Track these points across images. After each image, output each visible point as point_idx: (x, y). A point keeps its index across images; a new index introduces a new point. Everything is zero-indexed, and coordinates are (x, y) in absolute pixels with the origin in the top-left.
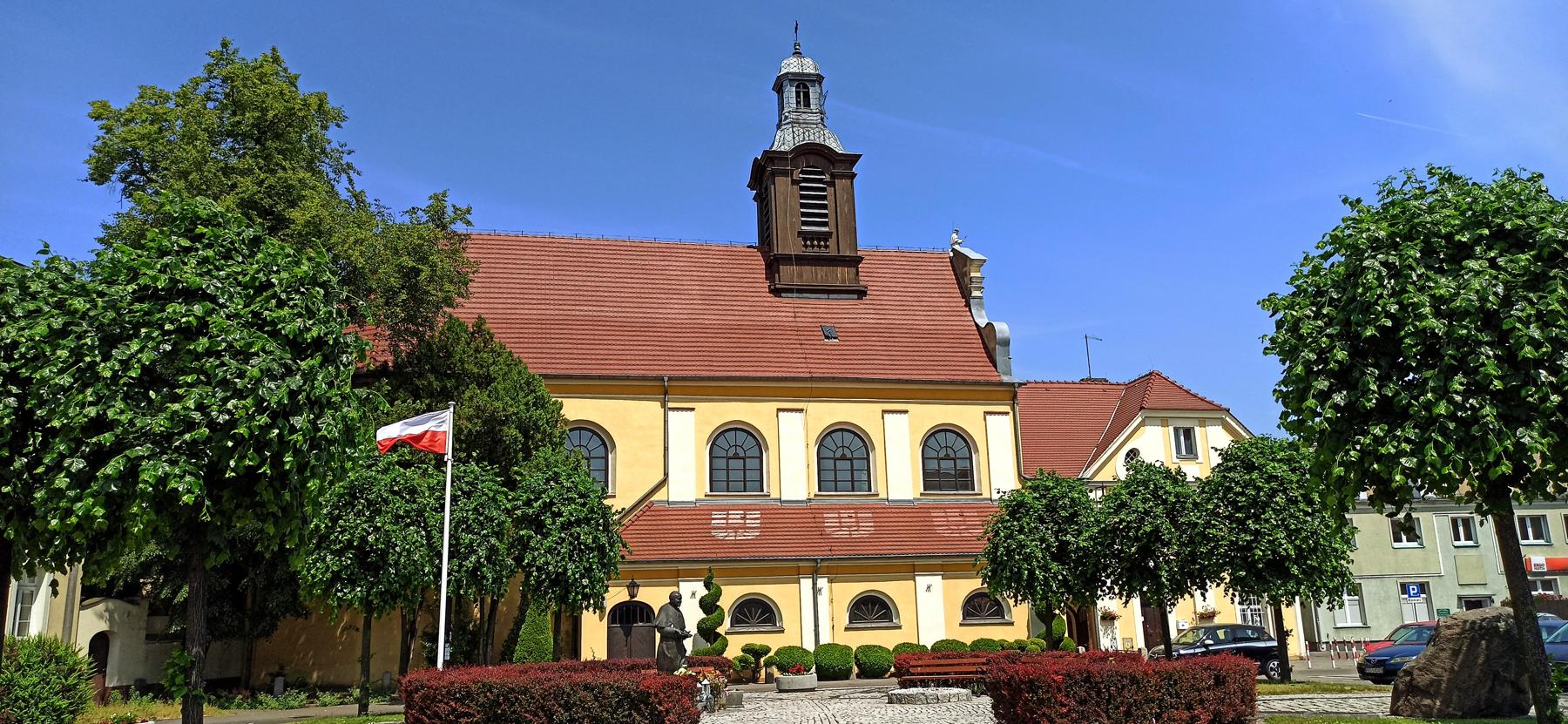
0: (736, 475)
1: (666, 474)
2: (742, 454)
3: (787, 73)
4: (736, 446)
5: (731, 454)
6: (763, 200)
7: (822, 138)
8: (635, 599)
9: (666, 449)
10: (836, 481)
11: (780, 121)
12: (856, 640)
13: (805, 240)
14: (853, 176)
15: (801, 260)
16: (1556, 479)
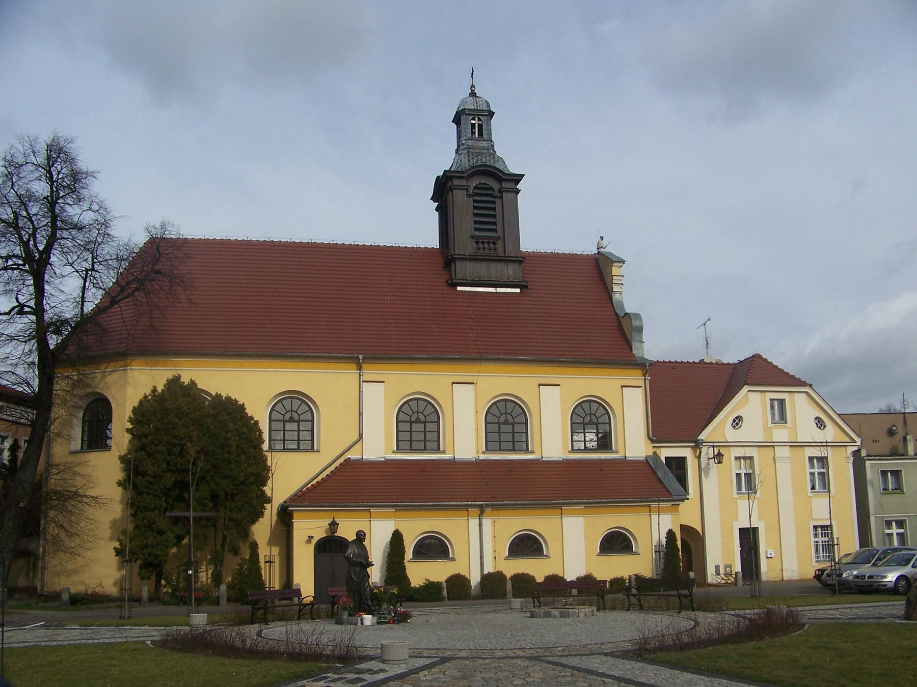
0: (507, 437)
1: (361, 436)
2: (511, 420)
3: (464, 109)
4: (590, 414)
5: (287, 417)
6: (443, 210)
7: (492, 161)
8: (336, 534)
9: (361, 414)
10: (500, 441)
11: (458, 146)
12: (512, 568)
13: (477, 243)
14: (518, 191)
15: (473, 259)
16: (392, 617)
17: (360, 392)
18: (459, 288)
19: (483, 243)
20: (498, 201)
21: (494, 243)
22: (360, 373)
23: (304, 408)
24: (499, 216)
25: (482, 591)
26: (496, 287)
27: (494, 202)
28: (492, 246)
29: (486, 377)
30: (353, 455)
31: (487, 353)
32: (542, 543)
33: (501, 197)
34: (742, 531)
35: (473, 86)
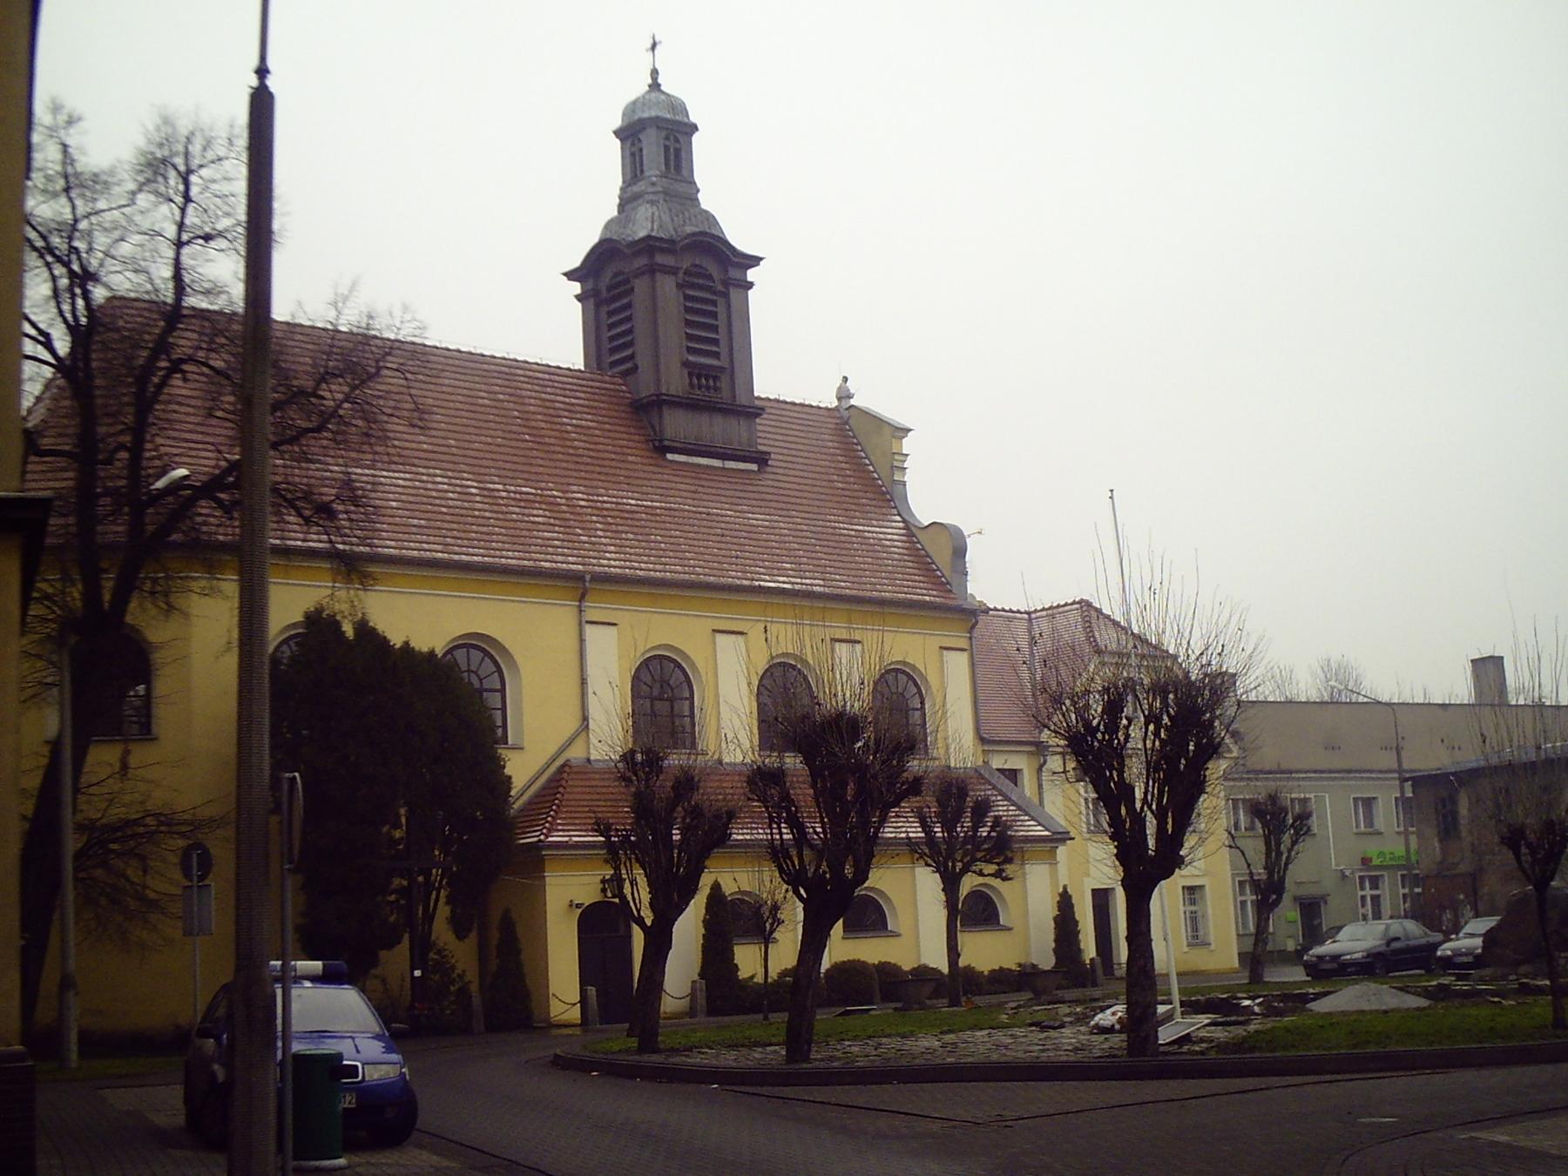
1: (585, 719)
17: (582, 641)
18: (669, 456)
19: (699, 377)
20: (721, 301)
21: (716, 378)
22: (580, 606)
23: (488, 666)
24: (722, 329)
25: (691, 1008)
26: (724, 459)
27: (714, 303)
28: (711, 383)
29: (423, 597)
30: (576, 753)
31: (1021, 613)
32: (988, 892)
33: (726, 295)
34: (1095, 892)
35: (655, 73)
